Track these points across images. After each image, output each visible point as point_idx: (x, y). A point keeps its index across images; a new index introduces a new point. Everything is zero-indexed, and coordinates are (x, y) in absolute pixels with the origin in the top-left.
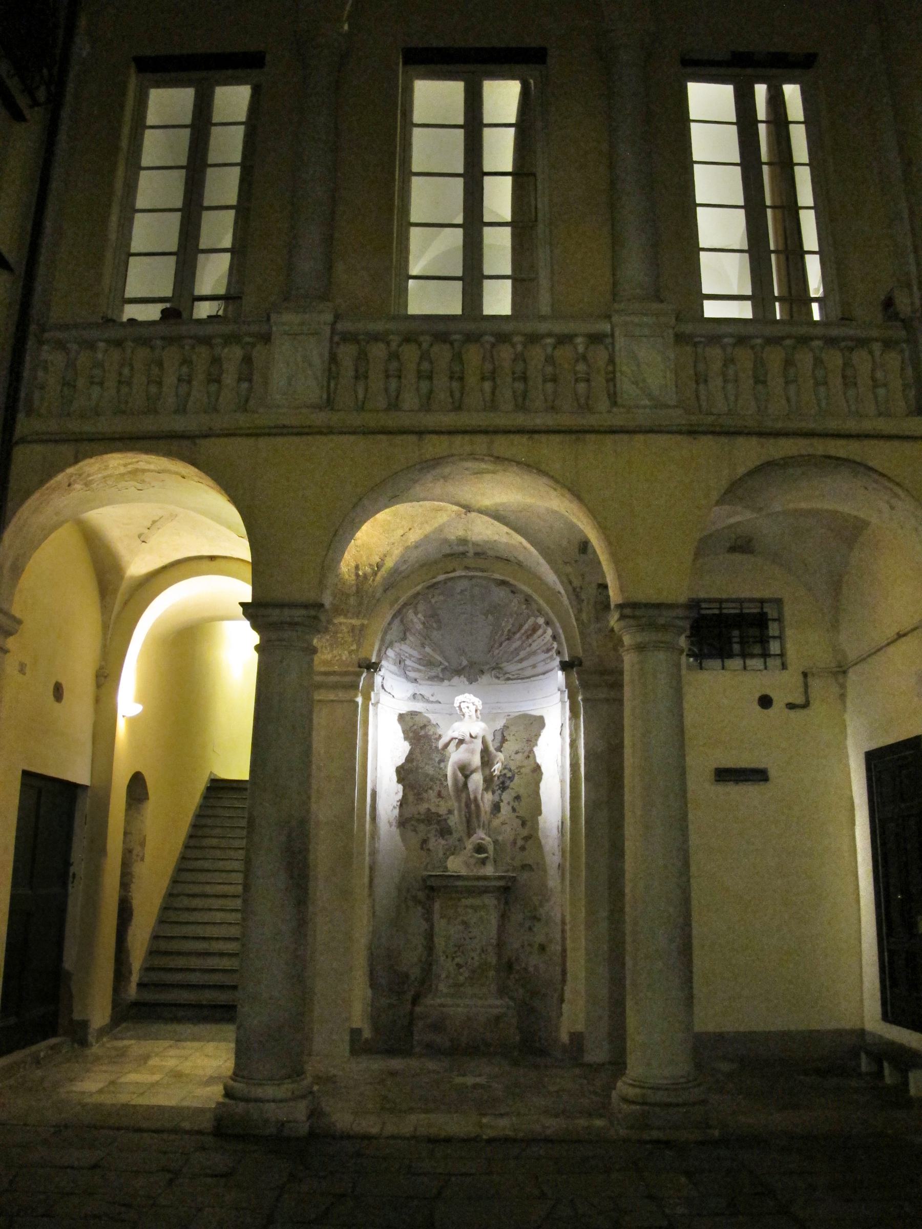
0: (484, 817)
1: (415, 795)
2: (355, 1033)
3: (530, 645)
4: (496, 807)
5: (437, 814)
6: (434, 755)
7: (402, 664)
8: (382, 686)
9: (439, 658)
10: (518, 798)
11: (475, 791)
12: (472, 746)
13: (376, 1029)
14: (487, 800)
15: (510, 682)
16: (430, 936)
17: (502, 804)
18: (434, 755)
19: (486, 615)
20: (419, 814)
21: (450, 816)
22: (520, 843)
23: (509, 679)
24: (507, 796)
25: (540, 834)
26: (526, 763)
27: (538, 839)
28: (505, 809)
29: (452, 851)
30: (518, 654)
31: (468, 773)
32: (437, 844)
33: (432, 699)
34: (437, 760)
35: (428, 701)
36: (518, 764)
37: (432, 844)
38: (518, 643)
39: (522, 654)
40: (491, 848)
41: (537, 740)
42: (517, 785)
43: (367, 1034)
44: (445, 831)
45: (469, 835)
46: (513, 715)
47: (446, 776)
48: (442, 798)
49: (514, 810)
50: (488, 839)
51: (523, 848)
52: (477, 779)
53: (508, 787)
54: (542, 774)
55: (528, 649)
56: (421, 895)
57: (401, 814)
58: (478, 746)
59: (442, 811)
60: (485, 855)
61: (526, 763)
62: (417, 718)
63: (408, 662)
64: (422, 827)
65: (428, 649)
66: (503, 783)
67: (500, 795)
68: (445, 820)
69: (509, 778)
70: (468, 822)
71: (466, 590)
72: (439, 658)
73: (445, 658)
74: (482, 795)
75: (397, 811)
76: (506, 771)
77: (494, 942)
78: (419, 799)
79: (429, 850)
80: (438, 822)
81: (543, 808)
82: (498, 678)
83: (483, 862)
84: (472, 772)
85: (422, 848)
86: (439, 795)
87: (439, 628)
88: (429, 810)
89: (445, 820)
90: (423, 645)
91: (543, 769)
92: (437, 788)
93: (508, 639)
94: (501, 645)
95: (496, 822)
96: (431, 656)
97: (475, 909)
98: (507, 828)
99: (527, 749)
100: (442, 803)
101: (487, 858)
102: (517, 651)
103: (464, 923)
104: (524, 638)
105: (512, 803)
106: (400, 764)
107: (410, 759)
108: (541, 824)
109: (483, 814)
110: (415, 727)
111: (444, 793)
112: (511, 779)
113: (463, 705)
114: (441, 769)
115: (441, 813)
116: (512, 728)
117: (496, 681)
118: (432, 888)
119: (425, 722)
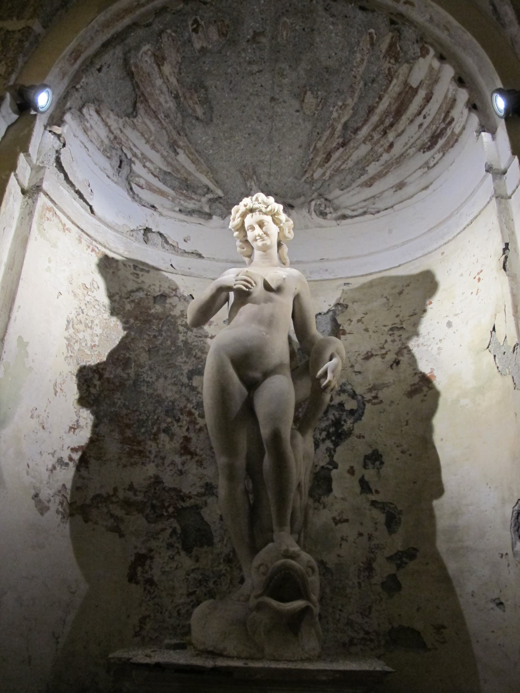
0: (297, 500)
1: (124, 441)
3: (391, 145)
4: (322, 481)
5: (177, 491)
6: (180, 360)
7: (125, 170)
8: (58, 161)
9: (205, 180)
10: (374, 458)
11: (275, 418)
12: (267, 309)
14: (303, 453)
15: (349, 221)
17: (334, 473)
18: (180, 360)
19: (300, 97)
20: (131, 487)
21: (210, 500)
22: (383, 569)
23: (344, 217)
24: (346, 455)
25: (442, 545)
26: (390, 376)
27: (437, 559)
28: (343, 485)
29: (207, 588)
30: (363, 171)
31: (257, 375)
32: (174, 568)
33: (183, 246)
34: (186, 368)
35: (175, 248)
36: (371, 378)
38: (364, 149)
39: (373, 169)
40: (314, 580)
41: (416, 325)
42: (371, 430)
44: (195, 537)
45: (254, 550)
46: (356, 283)
47: (200, 405)
48: (193, 454)
49: (365, 486)
50: (305, 556)
51: (392, 585)
52: (280, 391)
53: (349, 433)
54: (437, 394)
55: (386, 157)
57: (79, 485)
58: (286, 303)
59: (191, 485)
60: (298, 604)
61: (390, 376)
62: (147, 279)
63: (137, 168)
64: (137, 522)
65: (182, 157)
66: (337, 423)
67: (331, 453)
68: (196, 508)
69: (352, 412)
70: (254, 512)
71: (262, 33)
72: (205, 180)
73: (217, 182)
74: (293, 437)
75: (67, 476)
76: (344, 397)
78: (135, 451)
79: (150, 582)
80: (179, 513)
81: (448, 477)
82: (323, 215)
83: (294, 623)
84: (266, 375)
85: (132, 578)
86: (186, 450)
87: (208, 121)
88: (157, 481)
89: (196, 508)
90: (174, 146)
91: (439, 383)
92: (180, 432)
93: (343, 145)
94: (327, 159)
95: (322, 518)
96: (190, 174)
98: (348, 530)
99: (394, 347)
100: (192, 467)
101: (306, 610)
102: (362, 166)
104: (376, 136)
105: (359, 471)
106: (93, 361)
107: (119, 356)
108: (442, 522)
109: (293, 494)
110: (141, 294)
111: (197, 443)
112: (356, 414)
113: (249, 220)
114: (193, 389)
115: (186, 490)
116: (353, 307)
117: (320, 220)
119: (165, 289)
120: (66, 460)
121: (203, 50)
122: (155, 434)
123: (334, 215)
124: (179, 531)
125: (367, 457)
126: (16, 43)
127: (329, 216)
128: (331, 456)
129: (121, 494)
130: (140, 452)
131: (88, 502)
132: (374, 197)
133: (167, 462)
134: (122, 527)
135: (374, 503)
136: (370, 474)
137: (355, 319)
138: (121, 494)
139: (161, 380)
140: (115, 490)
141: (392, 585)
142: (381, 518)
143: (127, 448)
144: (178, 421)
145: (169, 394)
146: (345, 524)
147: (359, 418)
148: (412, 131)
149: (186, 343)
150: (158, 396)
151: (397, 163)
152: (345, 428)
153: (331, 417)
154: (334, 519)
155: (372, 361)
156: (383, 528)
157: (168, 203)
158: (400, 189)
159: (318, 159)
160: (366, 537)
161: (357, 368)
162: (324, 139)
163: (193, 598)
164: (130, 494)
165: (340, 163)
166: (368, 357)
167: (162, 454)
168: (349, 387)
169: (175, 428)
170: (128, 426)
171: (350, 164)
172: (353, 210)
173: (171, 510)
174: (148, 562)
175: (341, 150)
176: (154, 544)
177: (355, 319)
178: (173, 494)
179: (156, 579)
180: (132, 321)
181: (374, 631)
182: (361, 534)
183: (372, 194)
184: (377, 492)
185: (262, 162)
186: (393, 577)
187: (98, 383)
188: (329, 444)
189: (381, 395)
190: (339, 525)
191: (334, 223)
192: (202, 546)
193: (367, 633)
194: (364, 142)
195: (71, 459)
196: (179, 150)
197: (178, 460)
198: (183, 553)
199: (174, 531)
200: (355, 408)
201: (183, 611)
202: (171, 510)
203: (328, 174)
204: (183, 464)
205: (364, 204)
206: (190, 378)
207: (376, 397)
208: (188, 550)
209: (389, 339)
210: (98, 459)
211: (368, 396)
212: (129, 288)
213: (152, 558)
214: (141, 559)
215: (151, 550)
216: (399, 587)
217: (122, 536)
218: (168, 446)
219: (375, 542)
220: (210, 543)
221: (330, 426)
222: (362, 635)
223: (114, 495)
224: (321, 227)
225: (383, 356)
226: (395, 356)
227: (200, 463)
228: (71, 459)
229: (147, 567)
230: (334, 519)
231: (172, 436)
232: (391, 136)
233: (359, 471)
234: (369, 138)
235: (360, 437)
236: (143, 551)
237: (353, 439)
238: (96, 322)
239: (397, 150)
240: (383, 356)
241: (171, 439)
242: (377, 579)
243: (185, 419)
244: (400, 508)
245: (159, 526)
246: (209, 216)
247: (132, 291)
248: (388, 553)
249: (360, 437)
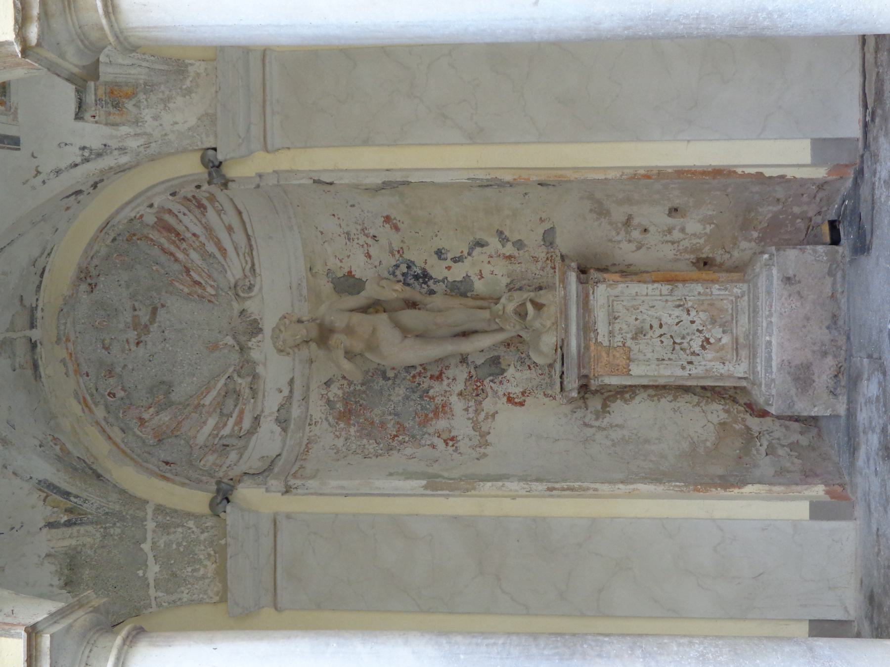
2: (818, 511)
3: (194, 235)
13: (808, 476)
16: (659, 390)
20: (466, 410)
30: (212, 255)
33: (286, 392)
35: (290, 397)
37: (515, 390)
38: (194, 255)
39: (211, 248)
43: (819, 491)
48: (441, 373)
56: (595, 403)
65: (207, 401)
69: (409, 267)
72: (222, 381)
76: (398, 273)
77: (666, 288)
79: (523, 393)
85: (521, 404)
94: (199, 283)
96: (219, 393)
97: (613, 318)
98: (487, 269)
102: (206, 256)
103: (639, 333)
104: (184, 245)
110: (330, 419)
118: (584, 388)
121: (123, 389)
122: (430, 398)
123: (251, 278)
124: (491, 378)
126: (168, 518)
127: (252, 282)
128: (439, 281)
129: (471, 415)
130: (443, 406)
131: (478, 433)
132: (236, 248)
133: (448, 389)
134: (491, 413)
137: (340, 264)
139: (392, 398)
140: (469, 419)
141: (519, 244)
142: (478, 249)
143: (441, 415)
144: (419, 384)
145: (401, 392)
147: (413, 263)
148: (186, 220)
149: (362, 384)
150: (403, 399)
151: (211, 231)
152: (419, 272)
153: (412, 281)
156: (485, 249)
157: (248, 408)
158: (232, 229)
159: (200, 291)
160: (490, 259)
162: (181, 287)
163: (532, 366)
164: (470, 409)
165: (204, 274)
166: (369, 256)
168: (391, 269)
169: (425, 386)
170: (427, 415)
171: (204, 266)
172: (247, 263)
173: (479, 384)
175: (192, 273)
176: (500, 393)
177: (340, 264)
182: (489, 262)
183: (233, 249)
185: (199, 336)
186: (514, 244)
187: (401, 437)
188: (431, 283)
189: (397, 249)
191: (258, 278)
192: (500, 363)
193: (547, 259)
194: (188, 255)
195: (453, 446)
197: (446, 382)
198: (505, 374)
199: (492, 381)
201: (540, 372)
202: (479, 384)
203: (213, 283)
204: (448, 378)
205: (241, 256)
206: (389, 379)
207: (399, 252)
208: (503, 371)
209: (356, 241)
210: (450, 431)
211: (397, 256)
212: (328, 426)
214: (510, 400)
215: (504, 395)
218: (437, 389)
220: (498, 357)
222: (549, 262)
223: (472, 419)
224: (261, 289)
227: (448, 367)
228: (453, 446)
229: (515, 396)
231: (431, 387)
232: (188, 235)
234: (185, 251)
236: (505, 399)
237: (427, 268)
238: (359, 443)
239: (198, 230)
241: (432, 387)
242: (515, 253)
243: (417, 379)
244: (472, 239)
245: (489, 390)
247: (329, 424)
248: (499, 246)
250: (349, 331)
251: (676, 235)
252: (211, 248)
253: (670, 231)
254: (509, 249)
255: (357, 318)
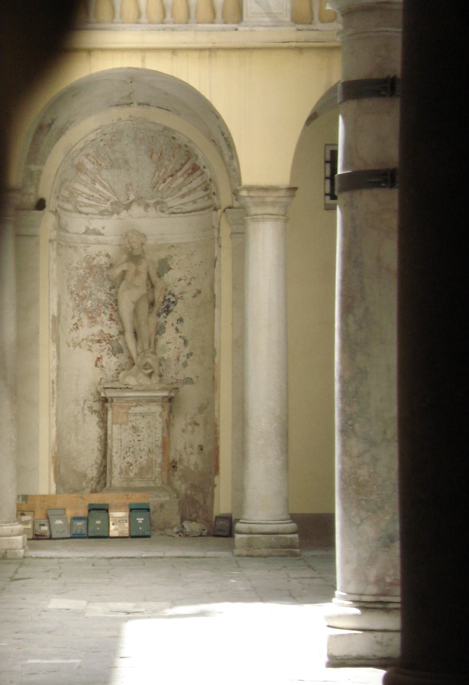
20: (93, 335)
22: (183, 359)
38: (181, 180)
39: (185, 190)
53: (171, 311)
69: (173, 302)
79: (102, 366)
85: (96, 365)
98: (172, 346)
105: (176, 325)
120: (72, 329)
124: (111, 349)
125: (178, 320)
127: (165, 212)
133: (105, 324)
134: (91, 348)
135: (180, 337)
136: (179, 326)
138: (90, 338)
140: (88, 336)
141: (185, 365)
142: (182, 341)
146: (171, 344)
154: (166, 342)
155: (181, 281)
156: (182, 345)
161: (175, 284)
166: (180, 280)
167: (103, 321)
168: (172, 292)
169: (107, 311)
174: (101, 360)
176: (102, 354)
178: (108, 335)
179: (104, 365)
180: (86, 270)
181: (100, 353)
182: (175, 348)
184: (181, 333)
190: (168, 344)
191: (167, 216)
193: (177, 380)
194: (180, 177)
196: (96, 183)
197: (109, 323)
198: (113, 356)
199: (109, 349)
200: (174, 300)
205: (180, 207)
208: (115, 355)
213: (102, 358)
214: (99, 359)
215: (101, 356)
216: (187, 365)
217: (92, 352)
219: (180, 350)
221: (165, 307)
223: (88, 338)
225: (185, 280)
226: (189, 281)
230: (166, 342)
231: (105, 314)
233: (176, 325)
235: (176, 312)
240: (185, 280)
242: (181, 362)
246: (112, 214)
249: (176, 312)
250: (137, 273)
251: (189, 450)
252: (185, 190)
253: (191, 446)
254: (183, 359)
255: (144, 277)
